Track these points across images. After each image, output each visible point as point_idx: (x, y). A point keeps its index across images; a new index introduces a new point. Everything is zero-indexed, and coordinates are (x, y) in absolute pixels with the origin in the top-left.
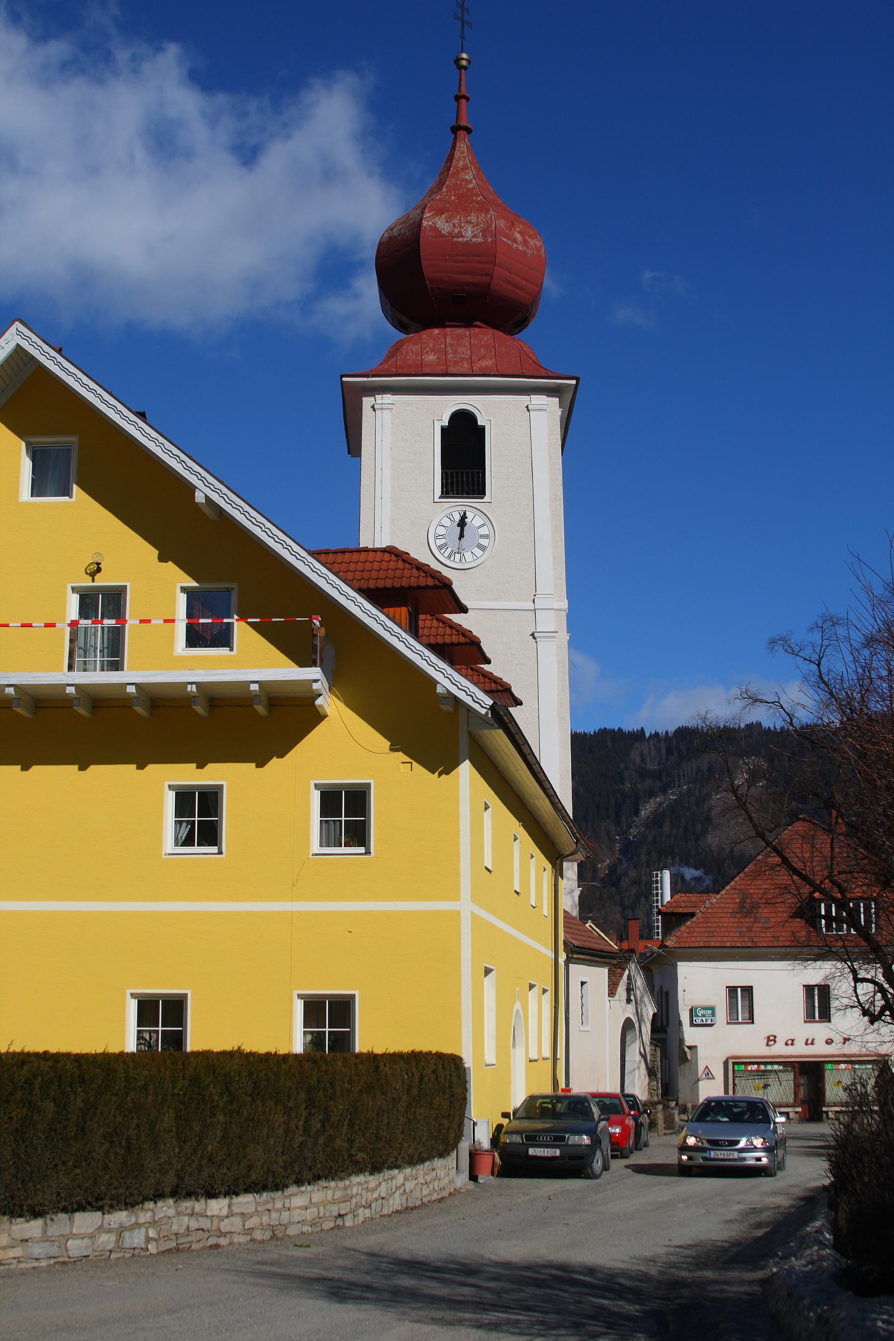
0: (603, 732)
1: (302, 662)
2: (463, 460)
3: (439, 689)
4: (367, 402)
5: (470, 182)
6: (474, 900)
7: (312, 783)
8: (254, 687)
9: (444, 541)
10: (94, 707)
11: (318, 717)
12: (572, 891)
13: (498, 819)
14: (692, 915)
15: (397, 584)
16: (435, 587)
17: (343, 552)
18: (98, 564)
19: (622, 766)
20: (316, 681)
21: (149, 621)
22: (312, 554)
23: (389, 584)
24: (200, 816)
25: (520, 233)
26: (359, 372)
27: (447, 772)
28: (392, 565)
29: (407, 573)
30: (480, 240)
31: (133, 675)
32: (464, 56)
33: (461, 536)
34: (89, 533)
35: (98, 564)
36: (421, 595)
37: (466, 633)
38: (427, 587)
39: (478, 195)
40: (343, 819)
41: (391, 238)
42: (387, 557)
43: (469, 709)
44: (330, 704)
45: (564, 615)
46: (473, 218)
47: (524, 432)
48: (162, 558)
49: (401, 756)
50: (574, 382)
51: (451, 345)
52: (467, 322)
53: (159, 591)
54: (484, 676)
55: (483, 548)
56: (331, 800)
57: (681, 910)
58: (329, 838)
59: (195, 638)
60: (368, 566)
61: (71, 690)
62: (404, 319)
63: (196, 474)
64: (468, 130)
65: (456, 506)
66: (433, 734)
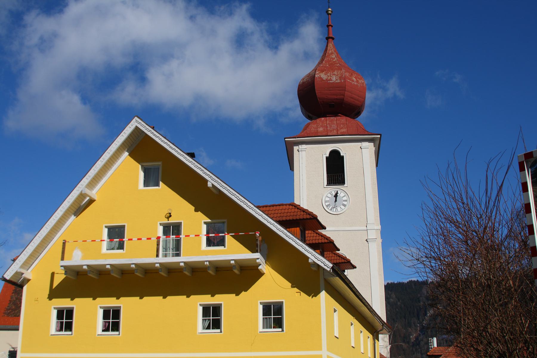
0: (411, 282)
1: (254, 251)
2: (335, 170)
3: (310, 261)
4: (296, 148)
5: (334, 59)
6: (329, 350)
7: (259, 302)
8: (232, 262)
9: (328, 203)
10: (169, 272)
11: (260, 274)
12: (387, 347)
13: (341, 316)
14: (441, 355)
15: (295, 218)
16: (310, 219)
17: (273, 206)
18: (170, 214)
19: (419, 295)
20: (258, 259)
21: (189, 236)
22: (258, 207)
23: (291, 218)
24: (213, 317)
25: (355, 78)
26: (292, 136)
27: (315, 295)
28: (293, 210)
29: (299, 213)
30: (339, 81)
31: (184, 258)
32: (330, 9)
33: (336, 201)
34: (167, 201)
35: (170, 214)
36: (306, 223)
37: (328, 238)
38: (307, 219)
39: (337, 64)
40: (272, 317)
41: (303, 83)
42: (291, 207)
43: (324, 269)
44: (265, 268)
45: (379, 232)
46: (335, 73)
47: (360, 158)
48: (196, 210)
49: (296, 290)
50: (379, 136)
51: (329, 124)
52: (335, 114)
53: (195, 224)
54: (339, 256)
55: (345, 205)
56: (267, 309)
57: (436, 354)
58: (266, 325)
59: (210, 242)
60: (283, 211)
61: (157, 265)
62: (310, 115)
63: (208, 175)
64: (333, 39)
65: (333, 189)
66: (308, 281)
